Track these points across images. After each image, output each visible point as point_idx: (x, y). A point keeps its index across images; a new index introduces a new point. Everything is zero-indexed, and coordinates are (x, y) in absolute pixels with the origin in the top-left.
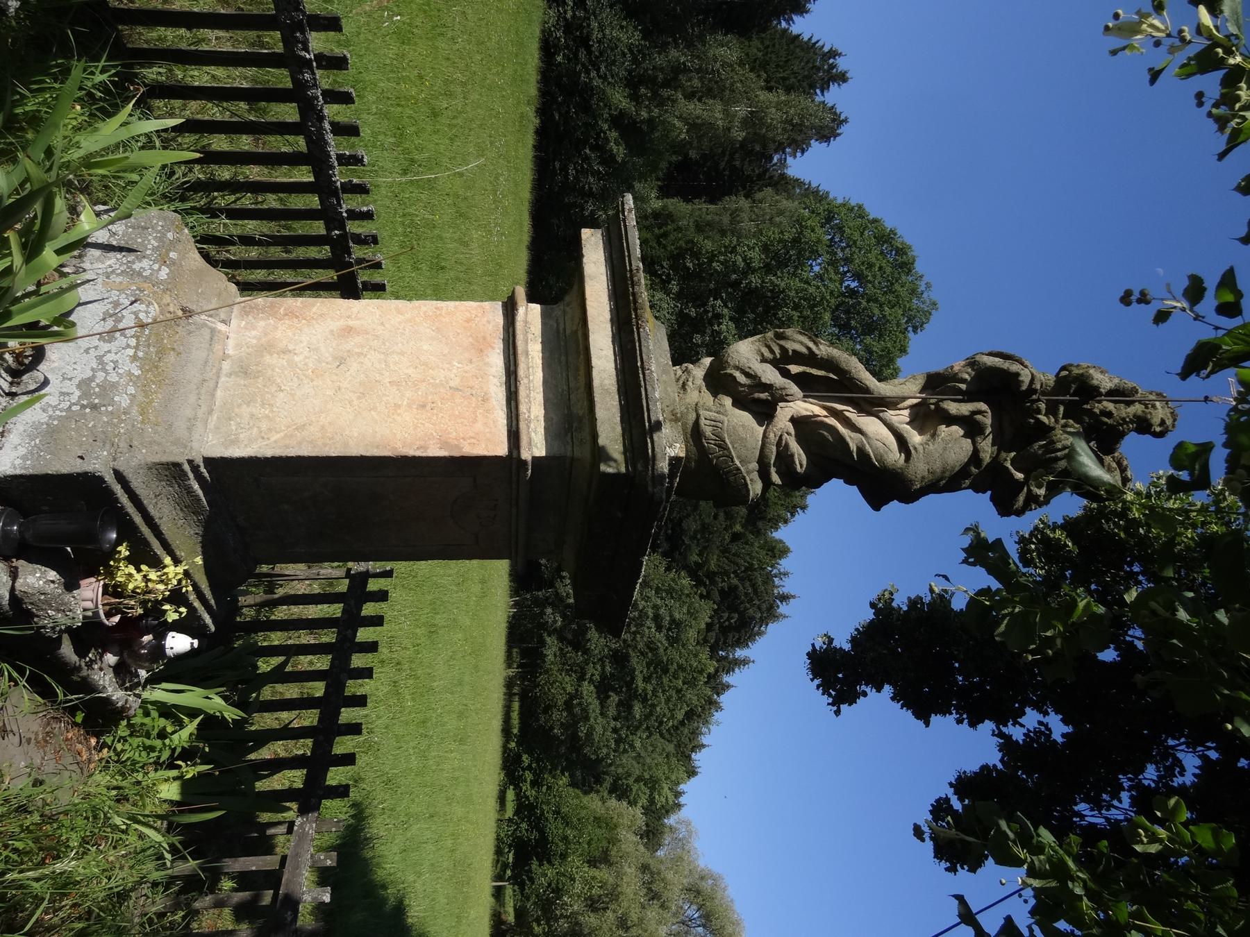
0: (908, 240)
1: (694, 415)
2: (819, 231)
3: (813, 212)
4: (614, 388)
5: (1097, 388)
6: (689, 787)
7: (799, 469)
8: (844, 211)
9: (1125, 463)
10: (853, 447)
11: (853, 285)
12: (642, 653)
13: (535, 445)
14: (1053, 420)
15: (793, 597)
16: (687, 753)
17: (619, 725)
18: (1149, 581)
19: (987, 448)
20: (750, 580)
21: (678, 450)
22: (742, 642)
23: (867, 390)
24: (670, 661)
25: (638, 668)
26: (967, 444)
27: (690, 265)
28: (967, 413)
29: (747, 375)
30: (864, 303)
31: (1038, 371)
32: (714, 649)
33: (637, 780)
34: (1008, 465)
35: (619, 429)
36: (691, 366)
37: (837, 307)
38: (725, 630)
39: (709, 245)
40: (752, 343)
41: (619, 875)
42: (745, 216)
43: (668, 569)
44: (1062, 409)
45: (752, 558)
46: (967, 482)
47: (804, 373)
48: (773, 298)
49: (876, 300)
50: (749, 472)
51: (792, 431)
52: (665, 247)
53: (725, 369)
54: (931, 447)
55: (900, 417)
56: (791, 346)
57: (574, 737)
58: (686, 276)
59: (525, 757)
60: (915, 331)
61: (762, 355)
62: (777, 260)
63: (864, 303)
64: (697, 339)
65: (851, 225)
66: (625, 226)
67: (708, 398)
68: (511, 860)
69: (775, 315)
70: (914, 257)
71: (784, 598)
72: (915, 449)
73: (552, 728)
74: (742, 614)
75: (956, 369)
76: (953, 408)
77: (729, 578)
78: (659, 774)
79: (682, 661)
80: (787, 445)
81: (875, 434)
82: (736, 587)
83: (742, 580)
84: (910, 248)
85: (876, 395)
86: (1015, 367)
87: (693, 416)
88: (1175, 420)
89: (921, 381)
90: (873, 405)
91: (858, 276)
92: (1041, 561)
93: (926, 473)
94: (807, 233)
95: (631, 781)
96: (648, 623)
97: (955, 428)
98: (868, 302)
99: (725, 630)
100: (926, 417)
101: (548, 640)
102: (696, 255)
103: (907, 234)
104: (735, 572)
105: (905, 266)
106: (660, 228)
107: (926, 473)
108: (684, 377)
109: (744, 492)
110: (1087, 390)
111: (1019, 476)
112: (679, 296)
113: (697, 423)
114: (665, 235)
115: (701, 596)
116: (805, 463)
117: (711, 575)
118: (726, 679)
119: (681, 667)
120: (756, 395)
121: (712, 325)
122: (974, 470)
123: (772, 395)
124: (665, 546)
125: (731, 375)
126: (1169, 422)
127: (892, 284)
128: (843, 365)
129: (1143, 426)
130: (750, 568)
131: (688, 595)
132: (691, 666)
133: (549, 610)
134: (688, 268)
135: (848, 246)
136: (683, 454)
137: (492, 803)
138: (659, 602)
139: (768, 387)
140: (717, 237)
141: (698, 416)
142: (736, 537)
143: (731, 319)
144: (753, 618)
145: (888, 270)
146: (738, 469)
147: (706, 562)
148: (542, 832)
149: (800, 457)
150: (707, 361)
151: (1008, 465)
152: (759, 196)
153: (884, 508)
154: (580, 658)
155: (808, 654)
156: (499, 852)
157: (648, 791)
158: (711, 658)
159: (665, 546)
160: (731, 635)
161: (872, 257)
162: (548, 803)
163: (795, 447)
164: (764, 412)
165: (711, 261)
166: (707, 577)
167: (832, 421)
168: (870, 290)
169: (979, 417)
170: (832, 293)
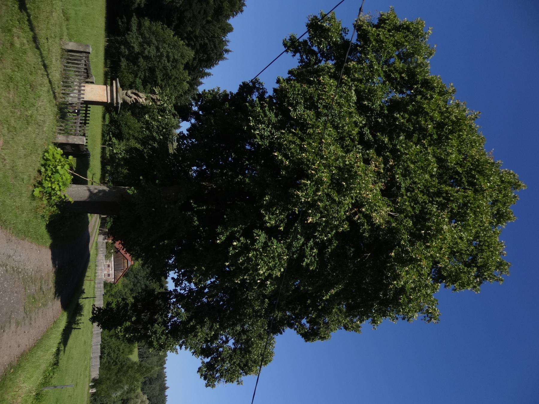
13: (109, 101)
15: (231, 51)
20: (213, 42)
25: (159, 76)
71: (227, 51)
77: (204, 39)
79: (177, 76)
82: (207, 44)
83: (210, 41)
96: (164, 58)
101: (122, 59)
104: (207, 37)
130: (213, 36)
133: (123, 47)
137: (101, 119)
138: (169, 50)
142: (208, 22)
148: (120, 130)
154: (136, 68)
156: (103, 136)
160: (203, 63)
162: (122, 121)
164: (131, 97)
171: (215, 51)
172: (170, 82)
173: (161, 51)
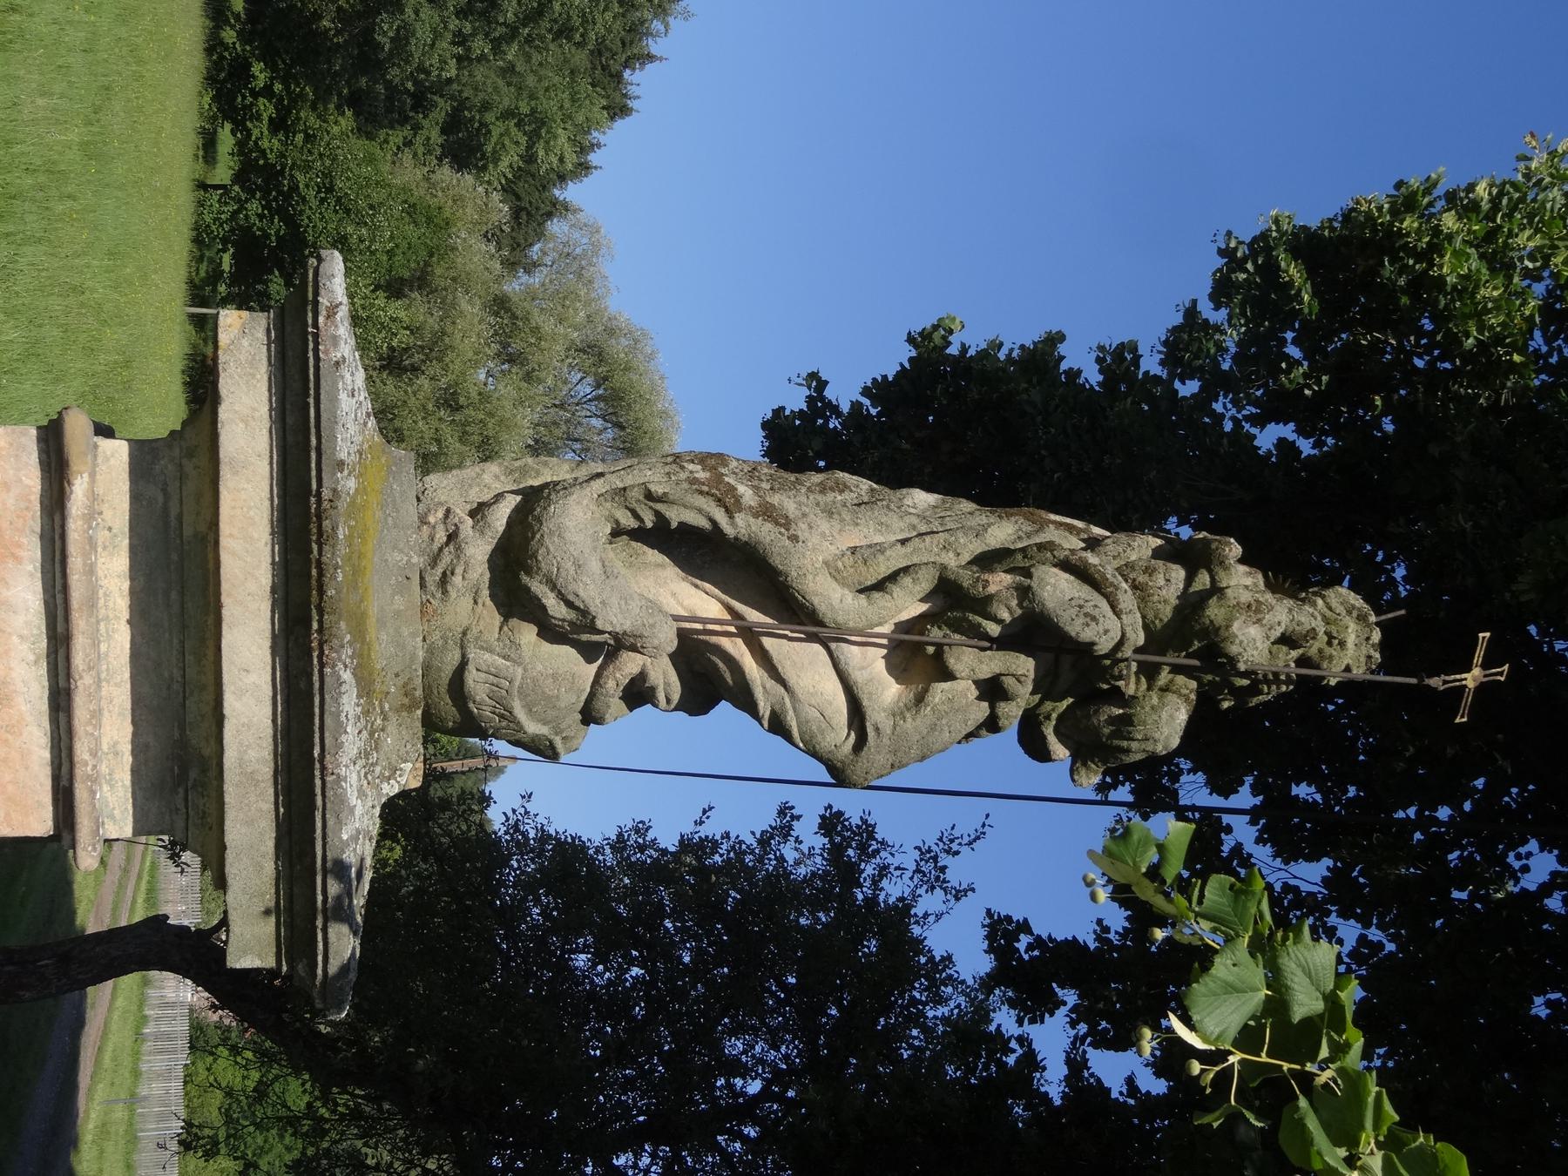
4: (267, 771)
6: (616, 143)
16: (615, 67)
17: (468, 28)
33: (508, 114)
35: (269, 867)
41: (449, 310)
57: (366, 40)
59: (257, 68)
66: (317, 359)
67: (491, 616)
68: (226, 266)
72: (877, 729)
73: (317, 16)
78: (549, 105)
87: (453, 658)
95: (490, 117)
128: (776, 561)
141: (463, 664)
148: (291, 222)
157: (523, 140)
162: (307, 167)
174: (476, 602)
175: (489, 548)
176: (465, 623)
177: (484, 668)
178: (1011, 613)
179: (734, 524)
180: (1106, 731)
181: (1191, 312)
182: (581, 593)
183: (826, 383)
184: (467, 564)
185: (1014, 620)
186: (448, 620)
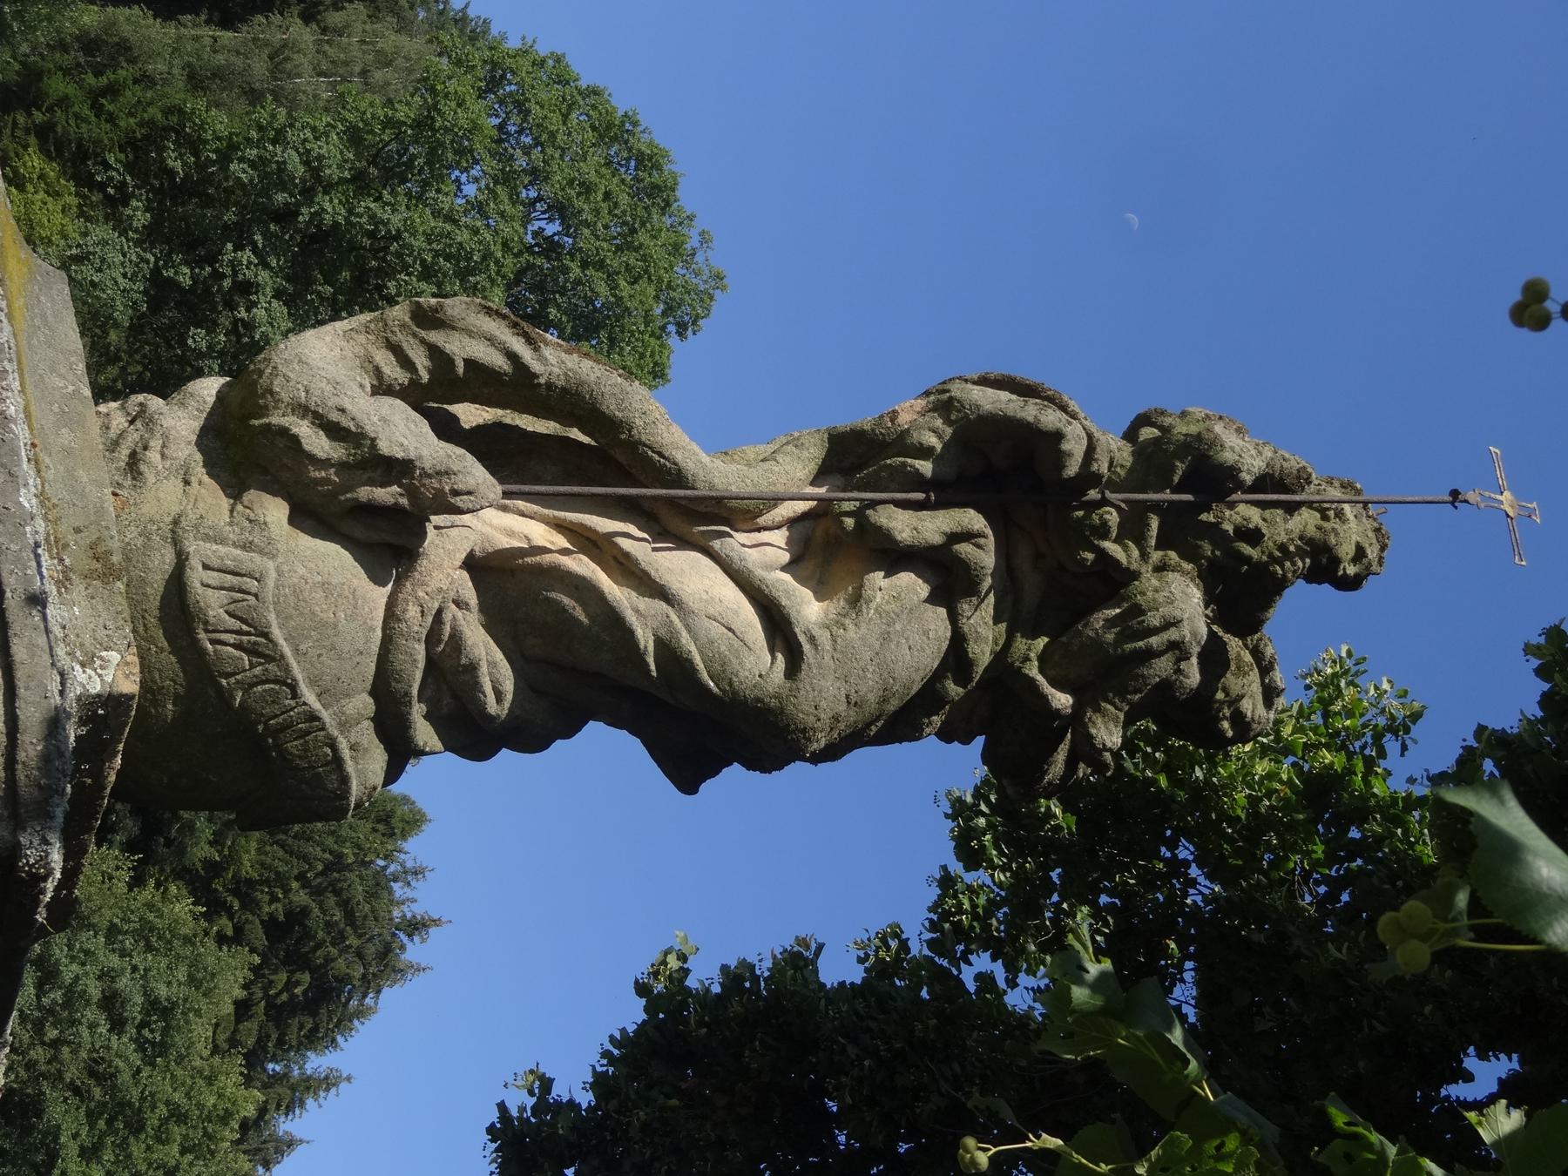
0: (662, 140)
1: (169, 556)
2: (476, 106)
3: (458, 63)
5: (1232, 472)
7: (492, 706)
8: (525, 64)
9: (1269, 651)
10: (645, 639)
11: (552, 229)
12: (77, 1091)
14: (1136, 553)
15: (436, 922)
18: (1211, 877)
19: (984, 628)
21: (113, 671)
22: (317, 1038)
23: (677, 477)
24: (150, 1100)
26: (937, 619)
27: (178, 166)
28: (937, 539)
29: (335, 431)
30: (576, 271)
31: (1092, 433)
32: (254, 1060)
34: (1033, 670)
36: (155, 403)
37: (520, 274)
38: (279, 1013)
39: (220, 123)
40: (347, 335)
42: (304, 62)
43: (137, 881)
44: (1154, 523)
45: (340, 841)
46: (937, 720)
47: (498, 426)
48: (374, 252)
49: (601, 265)
50: (344, 726)
51: (470, 594)
52: (111, 119)
53: (263, 411)
54: (852, 633)
55: (765, 552)
56: (460, 348)
58: (168, 192)
60: (682, 330)
61: (378, 372)
62: (386, 163)
63: (576, 271)
64: (198, 338)
65: (543, 96)
67: (211, 500)
69: (379, 288)
70: (674, 176)
71: (416, 927)
72: (812, 639)
74: (319, 973)
75: (905, 419)
76: (908, 525)
77: (287, 891)
80: (456, 640)
81: (702, 601)
82: (305, 911)
83: (317, 892)
84: (665, 154)
85: (703, 492)
86: (1051, 418)
88: (1383, 548)
89: (814, 452)
90: (693, 517)
91: (560, 210)
92: (1001, 853)
93: (842, 708)
94: (448, 107)
96: (92, 1014)
97: (907, 579)
98: (584, 265)
99: (279, 1013)
100: (835, 548)
102: (193, 145)
103: (659, 128)
104: (301, 877)
105: (659, 194)
106: (98, 74)
107: (842, 708)
108: (133, 437)
109: (332, 783)
110: (1213, 478)
111: (1062, 700)
112: (150, 236)
113: (177, 581)
114: (113, 91)
115: (221, 939)
116: (509, 686)
117: (244, 890)
118: (286, 1126)
119: (177, 1115)
120: (365, 493)
121: (231, 306)
122: (954, 690)
123: (412, 492)
124: (131, 826)
125: (284, 432)
126: (1372, 553)
127: (633, 231)
128: (610, 406)
129: (1323, 565)
130: (337, 864)
131: (187, 940)
132: (200, 1106)
134: (172, 173)
135: (537, 143)
136: (130, 686)
138: (115, 961)
139: (397, 469)
140: (241, 106)
141: (181, 560)
143: (278, 294)
144: (344, 980)
145: (624, 199)
146: (313, 717)
147: (232, 858)
149: (496, 674)
150: (208, 388)
151: (1033, 670)
152: (334, 18)
153: (707, 787)
155: (491, 1130)
158: (248, 1081)
159: (131, 826)
160: (294, 1023)
161: (589, 170)
163: (481, 646)
164: (389, 543)
165: (225, 158)
166: (235, 892)
167: (582, 565)
168: (586, 240)
169: (965, 549)
170: (506, 245)
171: (353, 941)
172: (137, 1150)
173: (67, 977)
174: (187, 483)
175: (196, 425)
176: (175, 509)
177: (215, 563)
178: (940, 437)
179: (542, 359)
180: (1110, 637)
181: (947, 882)
182: (348, 406)
183: (551, 1081)
184: (165, 436)
185: (946, 446)
186: (148, 509)
